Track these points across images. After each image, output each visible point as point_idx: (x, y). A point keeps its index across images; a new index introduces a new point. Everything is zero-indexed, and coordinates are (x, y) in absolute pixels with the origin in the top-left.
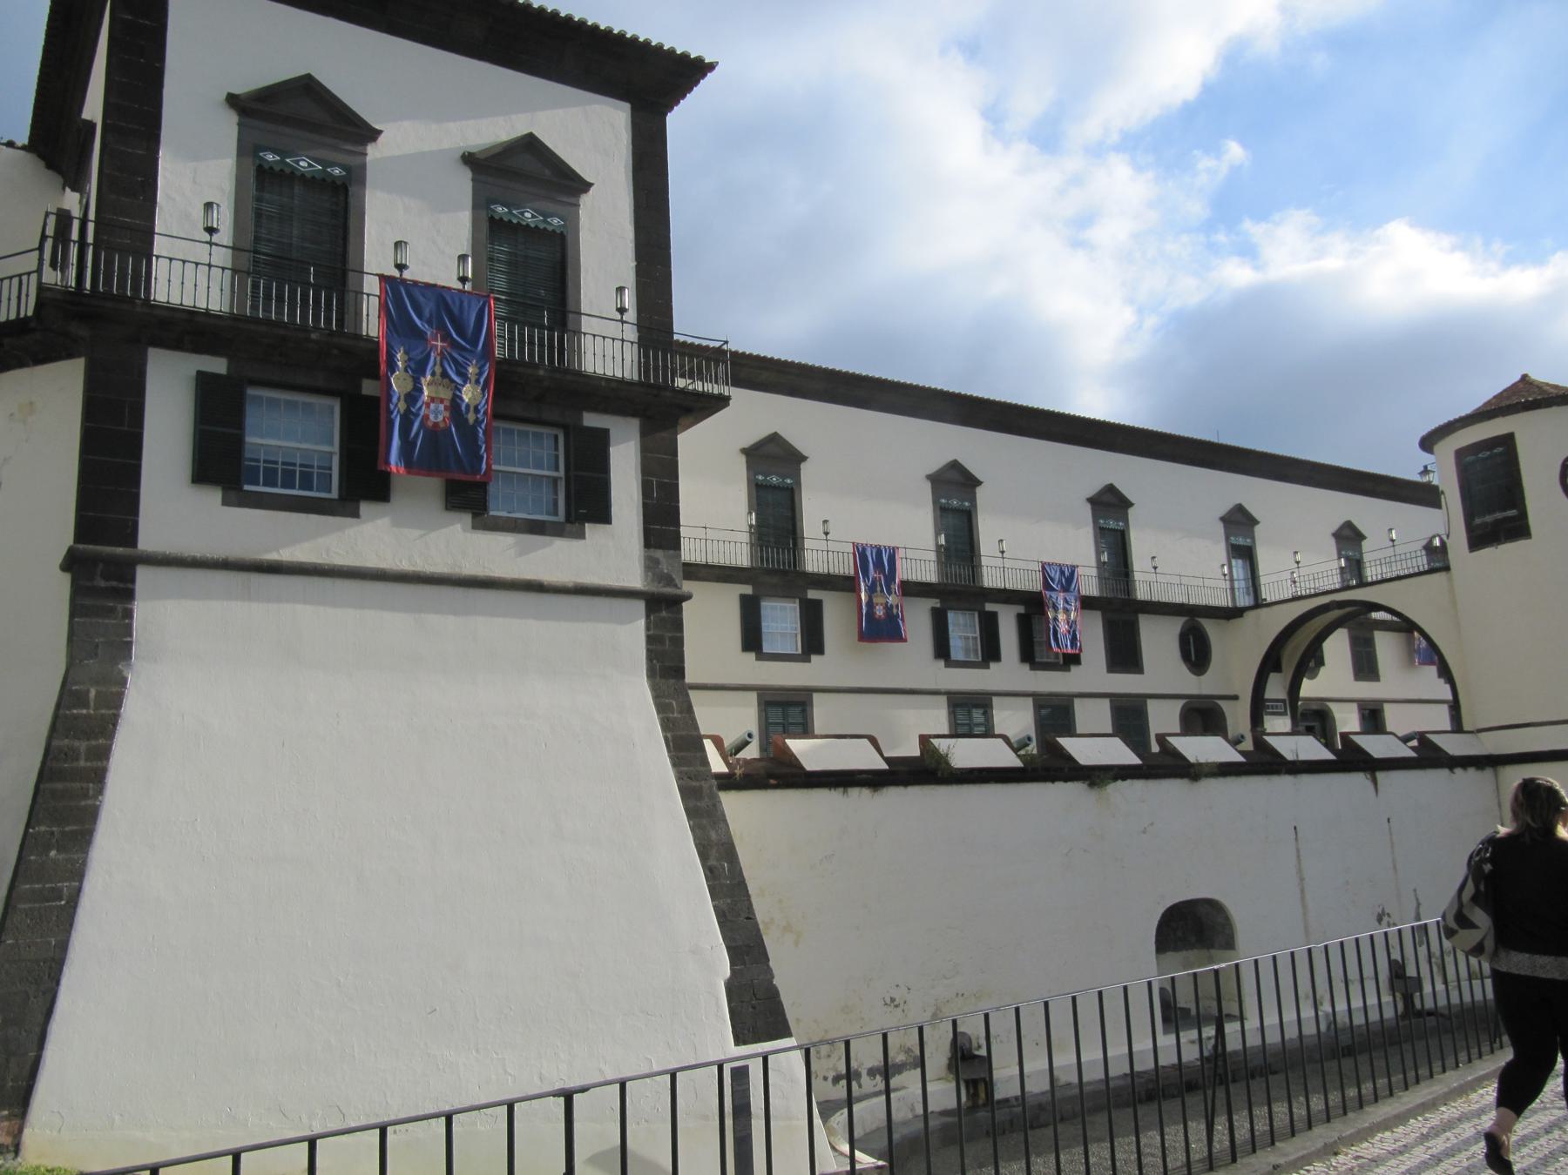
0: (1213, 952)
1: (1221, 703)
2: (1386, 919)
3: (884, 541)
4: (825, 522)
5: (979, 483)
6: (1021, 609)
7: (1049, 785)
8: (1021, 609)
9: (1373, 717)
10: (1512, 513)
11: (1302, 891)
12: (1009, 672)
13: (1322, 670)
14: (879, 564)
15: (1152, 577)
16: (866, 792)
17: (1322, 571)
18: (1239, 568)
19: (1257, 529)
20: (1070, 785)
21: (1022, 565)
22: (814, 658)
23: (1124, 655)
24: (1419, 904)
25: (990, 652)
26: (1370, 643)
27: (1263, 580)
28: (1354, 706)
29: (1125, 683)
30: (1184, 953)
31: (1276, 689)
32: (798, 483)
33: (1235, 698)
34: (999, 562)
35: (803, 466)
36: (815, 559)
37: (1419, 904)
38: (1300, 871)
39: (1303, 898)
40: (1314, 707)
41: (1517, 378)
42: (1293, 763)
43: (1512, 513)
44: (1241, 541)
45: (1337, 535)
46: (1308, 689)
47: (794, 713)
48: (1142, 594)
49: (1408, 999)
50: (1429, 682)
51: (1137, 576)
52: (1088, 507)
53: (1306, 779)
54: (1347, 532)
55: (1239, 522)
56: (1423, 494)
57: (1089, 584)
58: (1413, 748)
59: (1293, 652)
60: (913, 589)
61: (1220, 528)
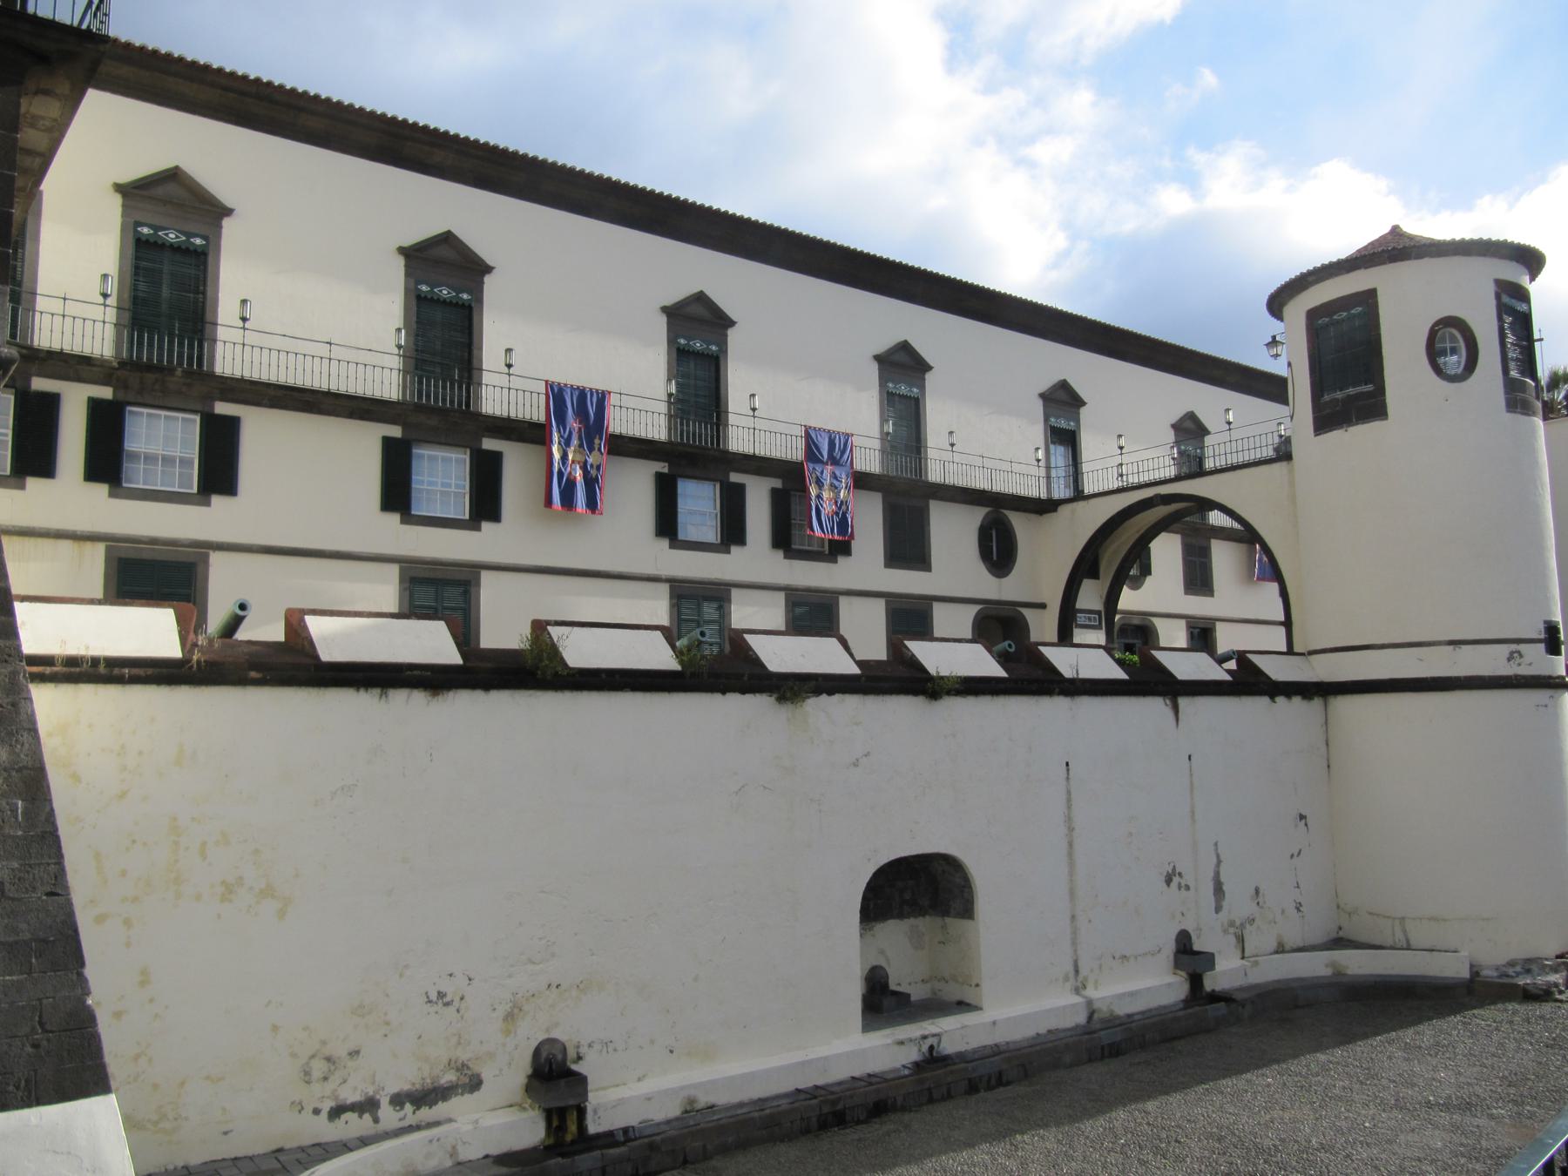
0: (948, 920)
1: (1026, 612)
2: (1176, 880)
3: (601, 387)
4: (509, 351)
5: (732, 323)
6: (777, 483)
7: (718, 697)
8: (777, 483)
9: (1202, 636)
10: (1370, 388)
11: (1071, 844)
12: (757, 558)
13: (1149, 579)
14: (581, 412)
15: (947, 456)
16: (418, 697)
17: (1154, 461)
18: (1060, 454)
19: (1083, 411)
20: (749, 698)
21: (781, 428)
22: (485, 525)
23: (908, 547)
24: (1219, 862)
25: (733, 532)
26: (1205, 553)
27: (1085, 468)
28: (1183, 623)
29: (907, 582)
30: (912, 921)
31: (1090, 597)
32: (480, 301)
33: (1043, 606)
34: (750, 422)
35: (487, 279)
36: (494, 400)
37: (1219, 862)
38: (1069, 819)
39: (1070, 855)
40: (1136, 621)
41: (1386, 230)
42: (1072, 681)
43: (1370, 388)
44: (1062, 424)
45: (1177, 427)
46: (1129, 600)
47: (452, 594)
48: (934, 474)
49: (1196, 981)
50: (1266, 600)
51: (931, 453)
52: (875, 366)
53: (1086, 703)
54: (1189, 424)
55: (1062, 401)
56: (1271, 388)
57: (868, 459)
58: (1229, 672)
59: (1113, 554)
60: (627, 447)
61: (1038, 406)
